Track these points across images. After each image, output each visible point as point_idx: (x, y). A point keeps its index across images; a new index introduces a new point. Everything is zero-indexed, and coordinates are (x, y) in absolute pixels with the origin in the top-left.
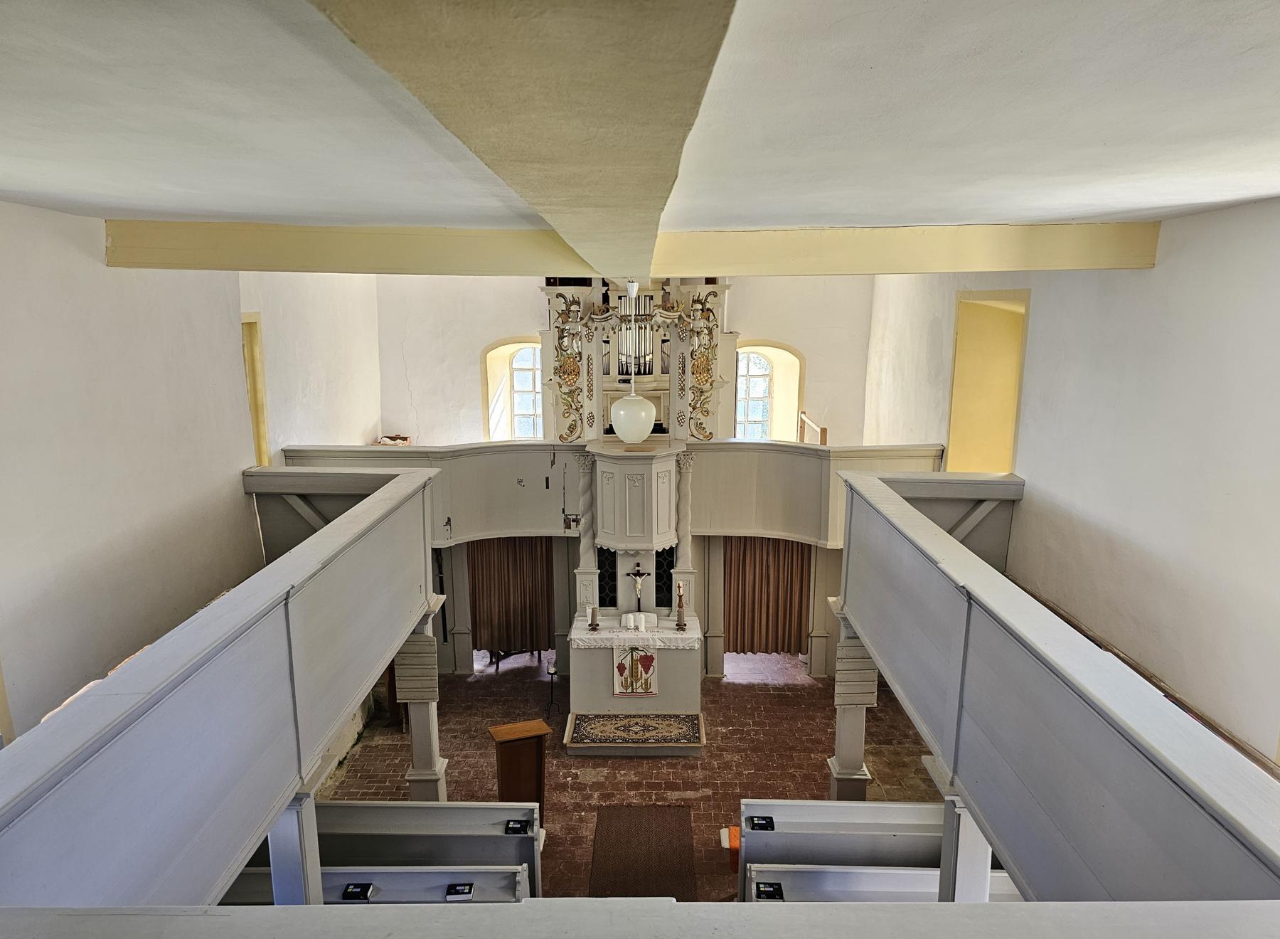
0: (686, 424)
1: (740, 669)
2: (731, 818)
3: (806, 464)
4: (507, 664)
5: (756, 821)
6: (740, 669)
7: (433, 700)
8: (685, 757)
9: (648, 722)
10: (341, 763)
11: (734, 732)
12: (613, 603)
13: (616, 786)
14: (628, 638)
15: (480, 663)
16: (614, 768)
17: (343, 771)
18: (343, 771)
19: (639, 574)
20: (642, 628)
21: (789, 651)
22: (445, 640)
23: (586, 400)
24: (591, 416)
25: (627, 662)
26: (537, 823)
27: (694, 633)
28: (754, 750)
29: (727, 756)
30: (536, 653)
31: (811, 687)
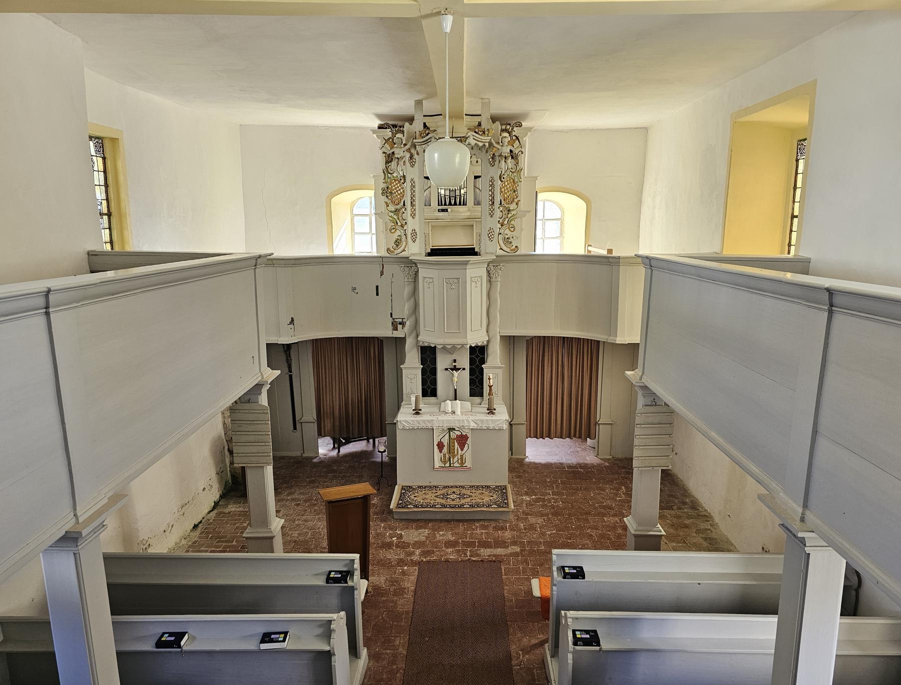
0: (495, 240)
1: (538, 451)
2: (542, 565)
3: (598, 272)
4: (346, 449)
5: (567, 570)
6: (538, 451)
7: (268, 464)
8: (495, 520)
9: (464, 491)
10: (196, 526)
11: (537, 500)
12: (434, 393)
13: (436, 544)
14: (445, 420)
15: (325, 448)
16: (434, 530)
17: (198, 532)
18: (198, 532)
19: (455, 369)
20: (458, 412)
21: (580, 437)
22: (295, 428)
23: (410, 219)
24: (414, 233)
25: (445, 441)
26: (357, 574)
27: (502, 416)
28: (555, 514)
29: (532, 520)
30: (371, 441)
31: (599, 465)
